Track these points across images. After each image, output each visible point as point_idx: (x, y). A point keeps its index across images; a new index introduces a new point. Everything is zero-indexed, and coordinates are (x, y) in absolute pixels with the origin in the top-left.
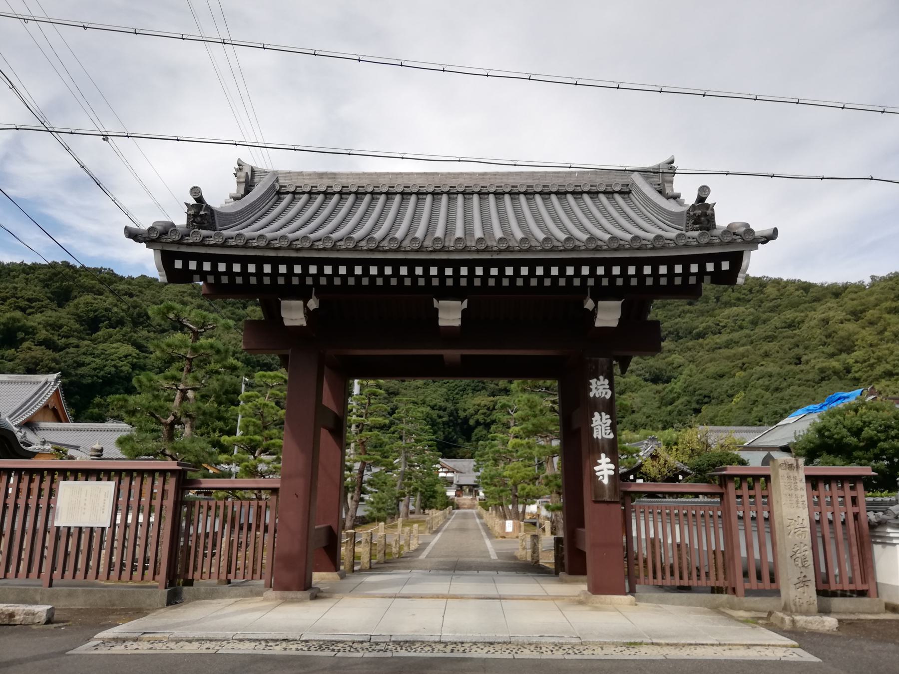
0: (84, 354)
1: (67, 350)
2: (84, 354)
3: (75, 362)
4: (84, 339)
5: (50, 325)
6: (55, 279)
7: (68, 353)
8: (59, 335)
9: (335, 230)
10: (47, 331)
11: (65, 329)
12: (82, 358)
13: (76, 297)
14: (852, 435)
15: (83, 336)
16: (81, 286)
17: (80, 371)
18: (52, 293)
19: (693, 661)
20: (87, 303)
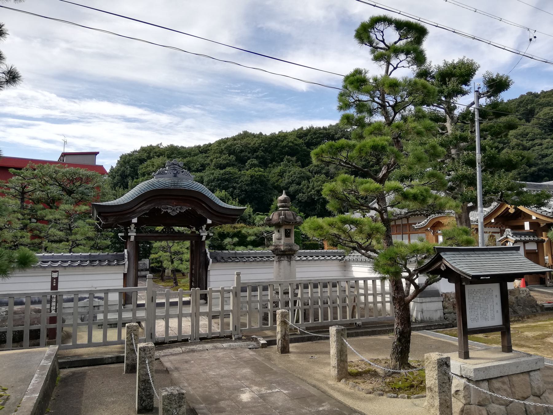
0: (546, 148)
1: (534, 148)
2: (546, 148)
3: (540, 155)
4: (545, 139)
5: (520, 135)
6: (521, 105)
7: (533, 150)
8: (527, 140)
9: (138, 208)
10: (518, 139)
11: (530, 135)
12: (546, 152)
13: (538, 112)
14: (231, 144)
15: (544, 136)
16: (540, 105)
17: (544, 161)
18: (521, 115)
19: (109, 99)
20: (546, 114)
